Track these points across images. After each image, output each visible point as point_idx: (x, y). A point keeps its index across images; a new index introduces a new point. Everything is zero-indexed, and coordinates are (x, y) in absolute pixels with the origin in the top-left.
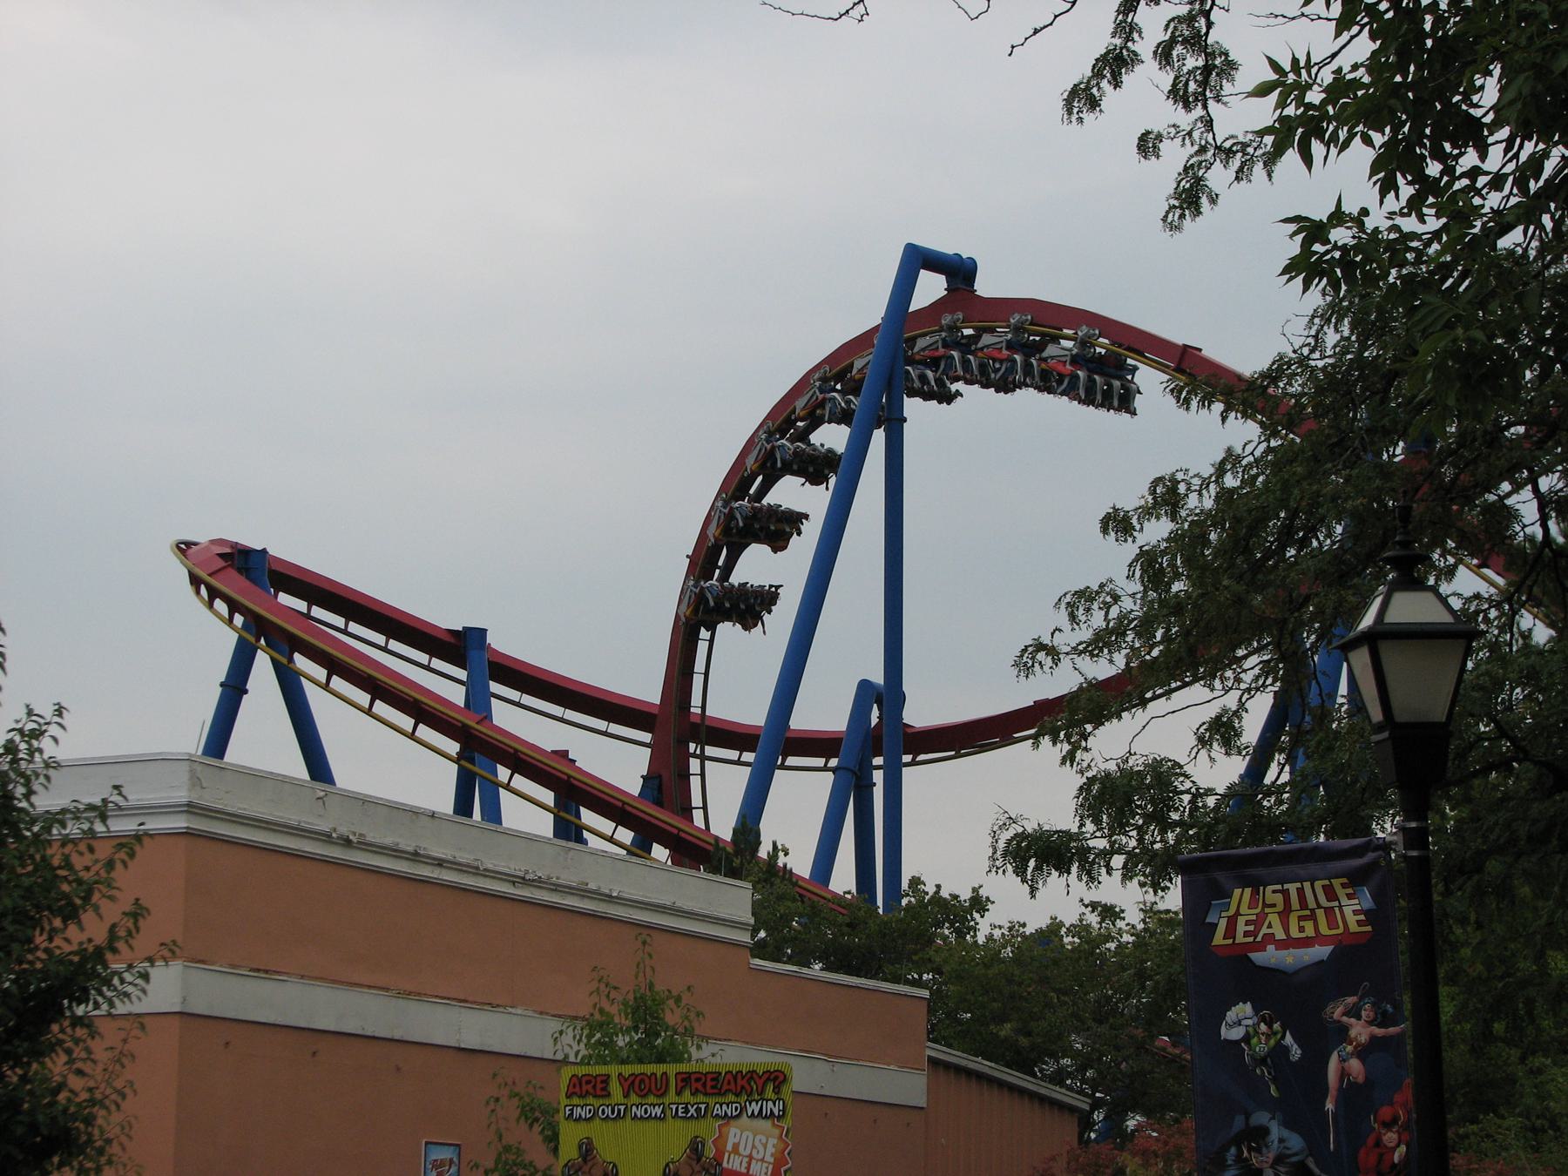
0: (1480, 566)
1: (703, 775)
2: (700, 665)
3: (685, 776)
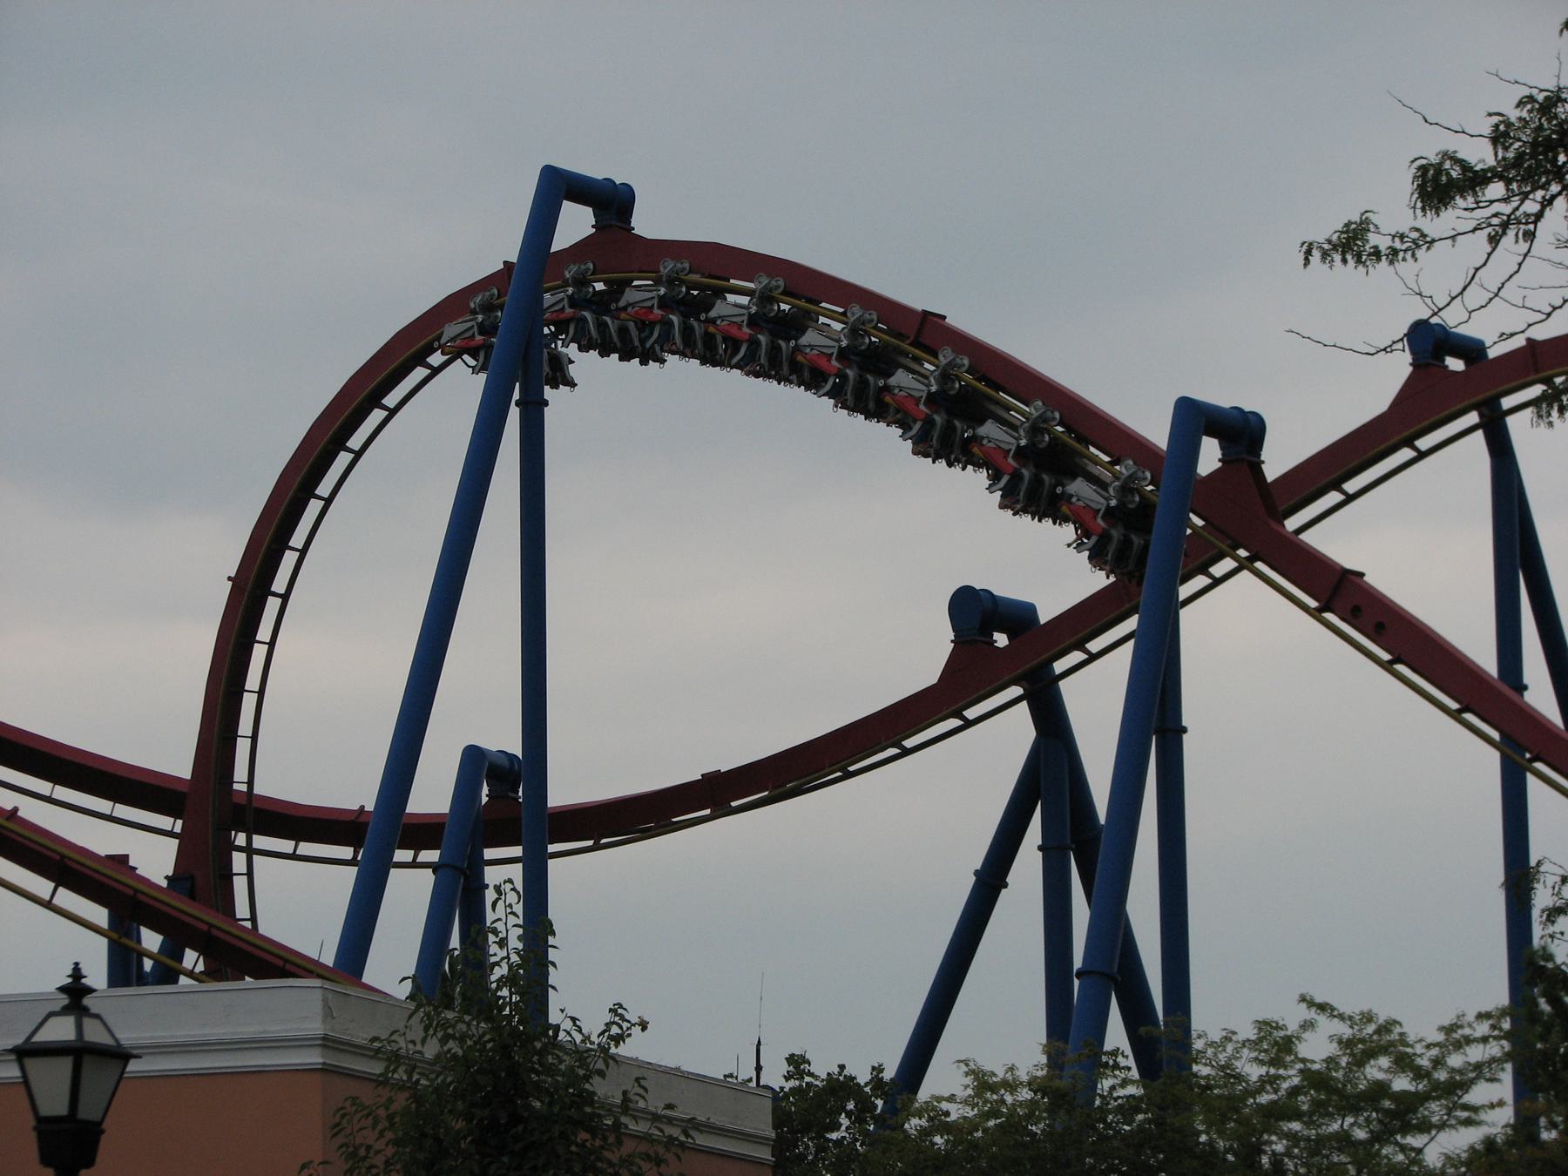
0: (1320, 610)
1: (250, 874)
2: (245, 727)
3: (227, 876)
